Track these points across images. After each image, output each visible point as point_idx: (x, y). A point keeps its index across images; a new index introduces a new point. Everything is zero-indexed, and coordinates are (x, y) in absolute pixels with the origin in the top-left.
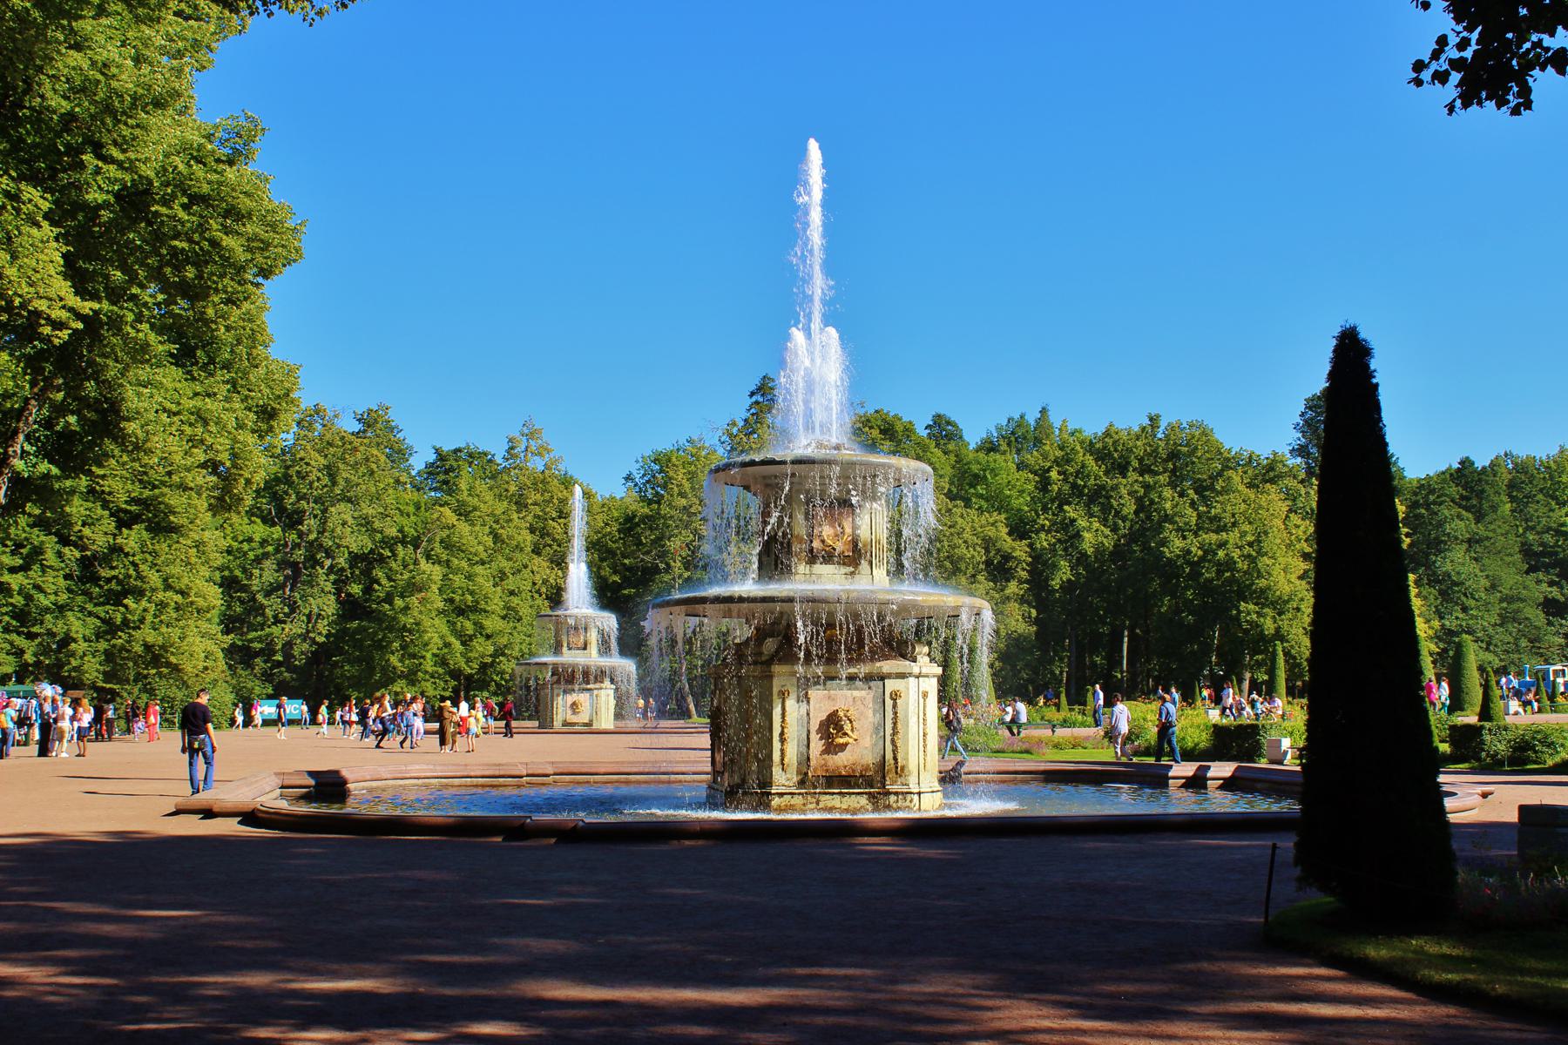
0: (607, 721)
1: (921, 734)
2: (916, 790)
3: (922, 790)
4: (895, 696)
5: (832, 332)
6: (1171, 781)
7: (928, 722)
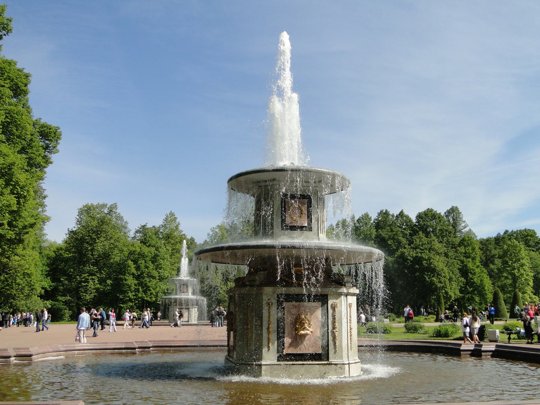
0: (194, 321)
1: (349, 329)
2: (348, 362)
3: (350, 362)
4: (334, 308)
5: (295, 96)
6: (226, 324)
7: (352, 321)
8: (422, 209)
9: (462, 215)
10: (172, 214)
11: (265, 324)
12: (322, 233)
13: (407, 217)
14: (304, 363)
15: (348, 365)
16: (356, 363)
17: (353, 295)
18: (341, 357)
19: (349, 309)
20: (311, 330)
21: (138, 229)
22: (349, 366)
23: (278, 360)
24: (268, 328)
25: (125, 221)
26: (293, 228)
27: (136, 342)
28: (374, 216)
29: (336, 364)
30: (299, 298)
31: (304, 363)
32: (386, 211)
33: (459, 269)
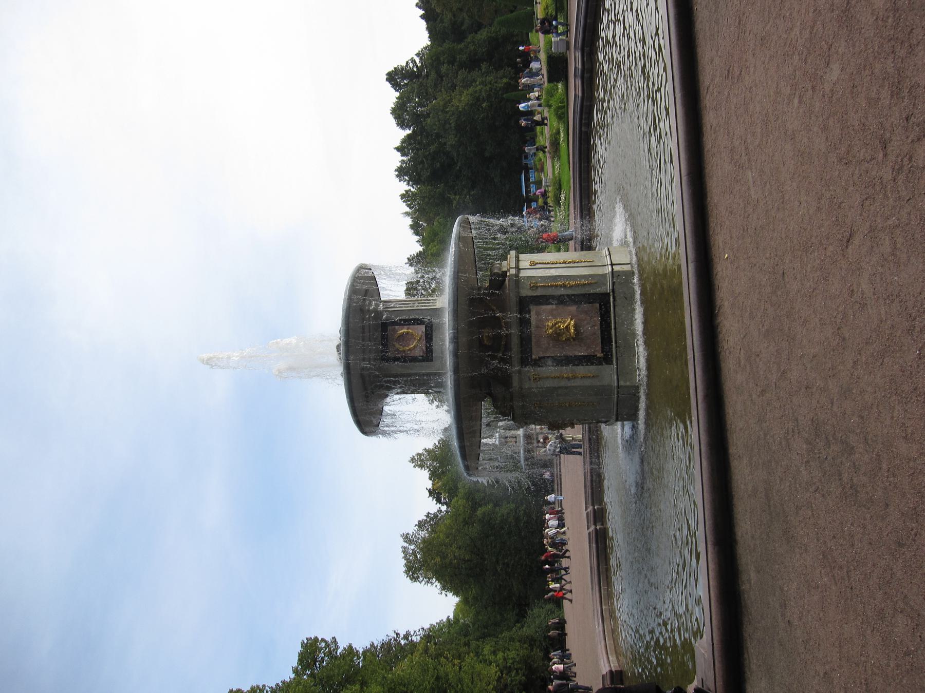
2: (610, 267)
3: (609, 263)
8: (392, 121)
9: (398, 66)
10: (413, 460)
11: (563, 383)
12: (436, 302)
13: (403, 141)
14: (613, 328)
15: (614, 267)
16: (610, 254)
17: (518, 260)
18: (604, 276)
19: (538, 266)
20: (569, 320)
21: (435, 502)
22: (614, 265)
23: (611, 363)
24: (568, 378)
25: (425, 518)
26: (429, 351)
27: (588, 528)
28: (403, 187)
29: (613, 283)
30: (525, 341)
31: (613, 328)
32: (396, 171)
33: (469, 72)
